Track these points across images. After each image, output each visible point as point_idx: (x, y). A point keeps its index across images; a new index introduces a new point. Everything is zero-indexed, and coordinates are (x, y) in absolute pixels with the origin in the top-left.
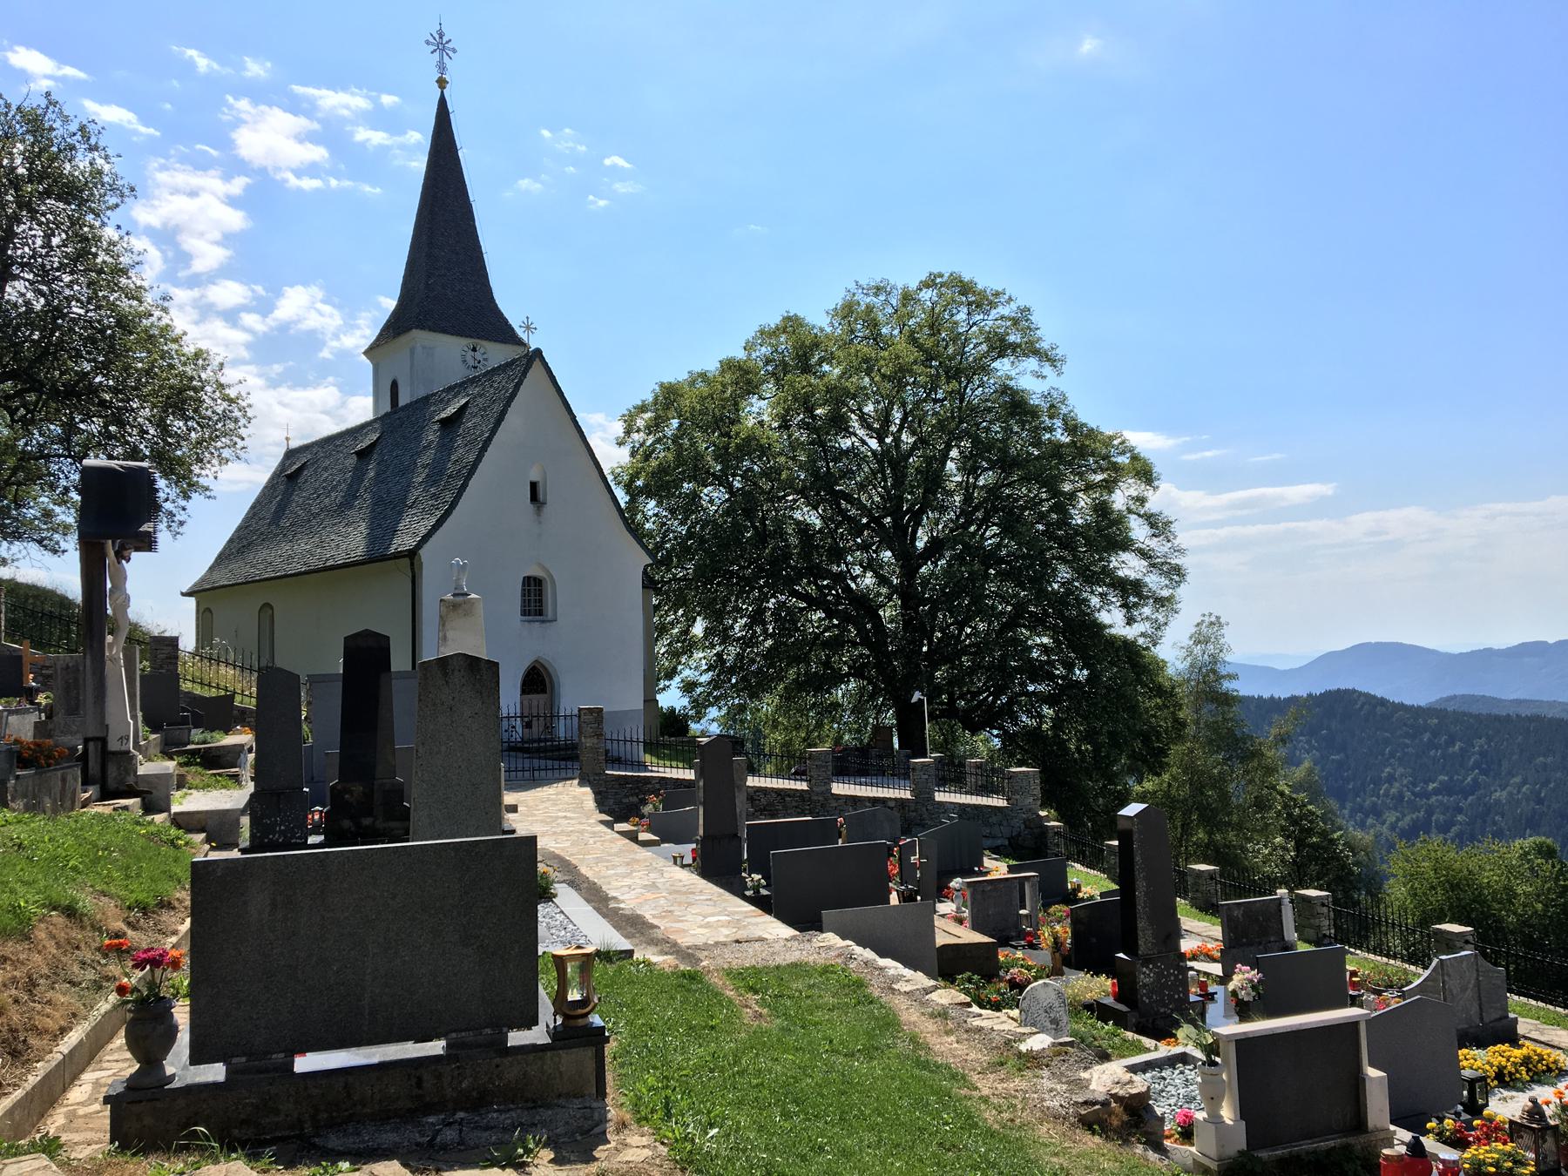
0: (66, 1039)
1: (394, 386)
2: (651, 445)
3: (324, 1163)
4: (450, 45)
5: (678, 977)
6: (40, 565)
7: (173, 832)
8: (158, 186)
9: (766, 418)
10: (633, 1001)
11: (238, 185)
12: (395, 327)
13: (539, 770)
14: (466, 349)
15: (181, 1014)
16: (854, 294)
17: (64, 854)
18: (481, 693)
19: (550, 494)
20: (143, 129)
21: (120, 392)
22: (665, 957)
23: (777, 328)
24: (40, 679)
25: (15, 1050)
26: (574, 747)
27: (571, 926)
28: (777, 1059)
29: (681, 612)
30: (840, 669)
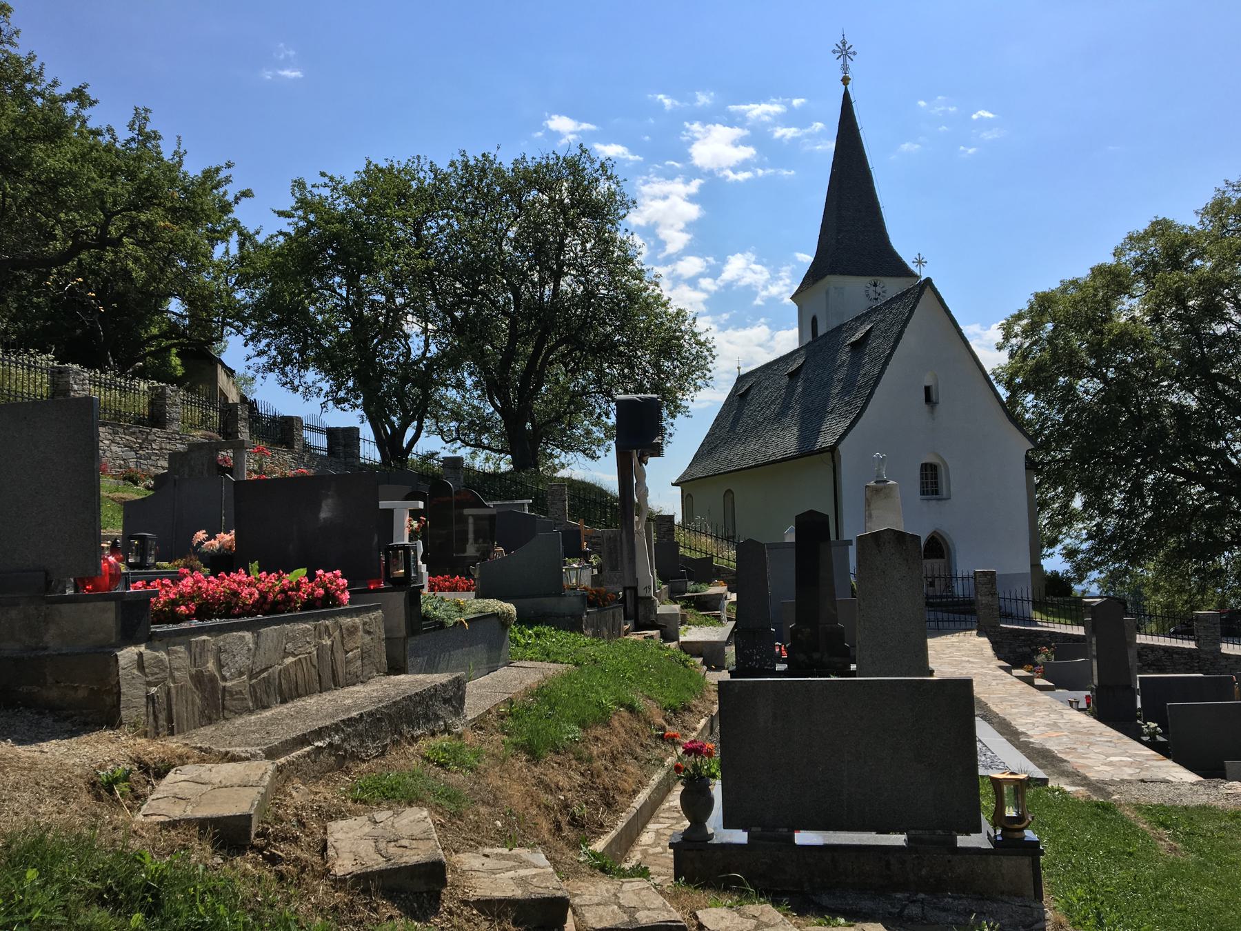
0: (637, 798)
1: (814, 321)
2: (1028, 347)
3: (827, 917)
4: (837, 55)
5: (1091, 807)
6: (585, 467)
7: (683, 656)
8: (643, 196)
9: (1137, 314)
10: (1053, 822)
11: (694, 186)
12: (814, 275)
13: (943, 621)
14: (869, 285)
15: (716, 790)
16: (1224, 193)
17: (623, 669)
18: (907, 561)
19: (941, 396)
20: (631, 157)
21: (631, 345)
22: (1078, 788)
23: (1146, 232)
24: (590, 545)
25: (608, 802)
26: (971, 603)
27: (989, 753)
28: (1197, 890)
29: (1060, 489)
30: (1223, 538)
